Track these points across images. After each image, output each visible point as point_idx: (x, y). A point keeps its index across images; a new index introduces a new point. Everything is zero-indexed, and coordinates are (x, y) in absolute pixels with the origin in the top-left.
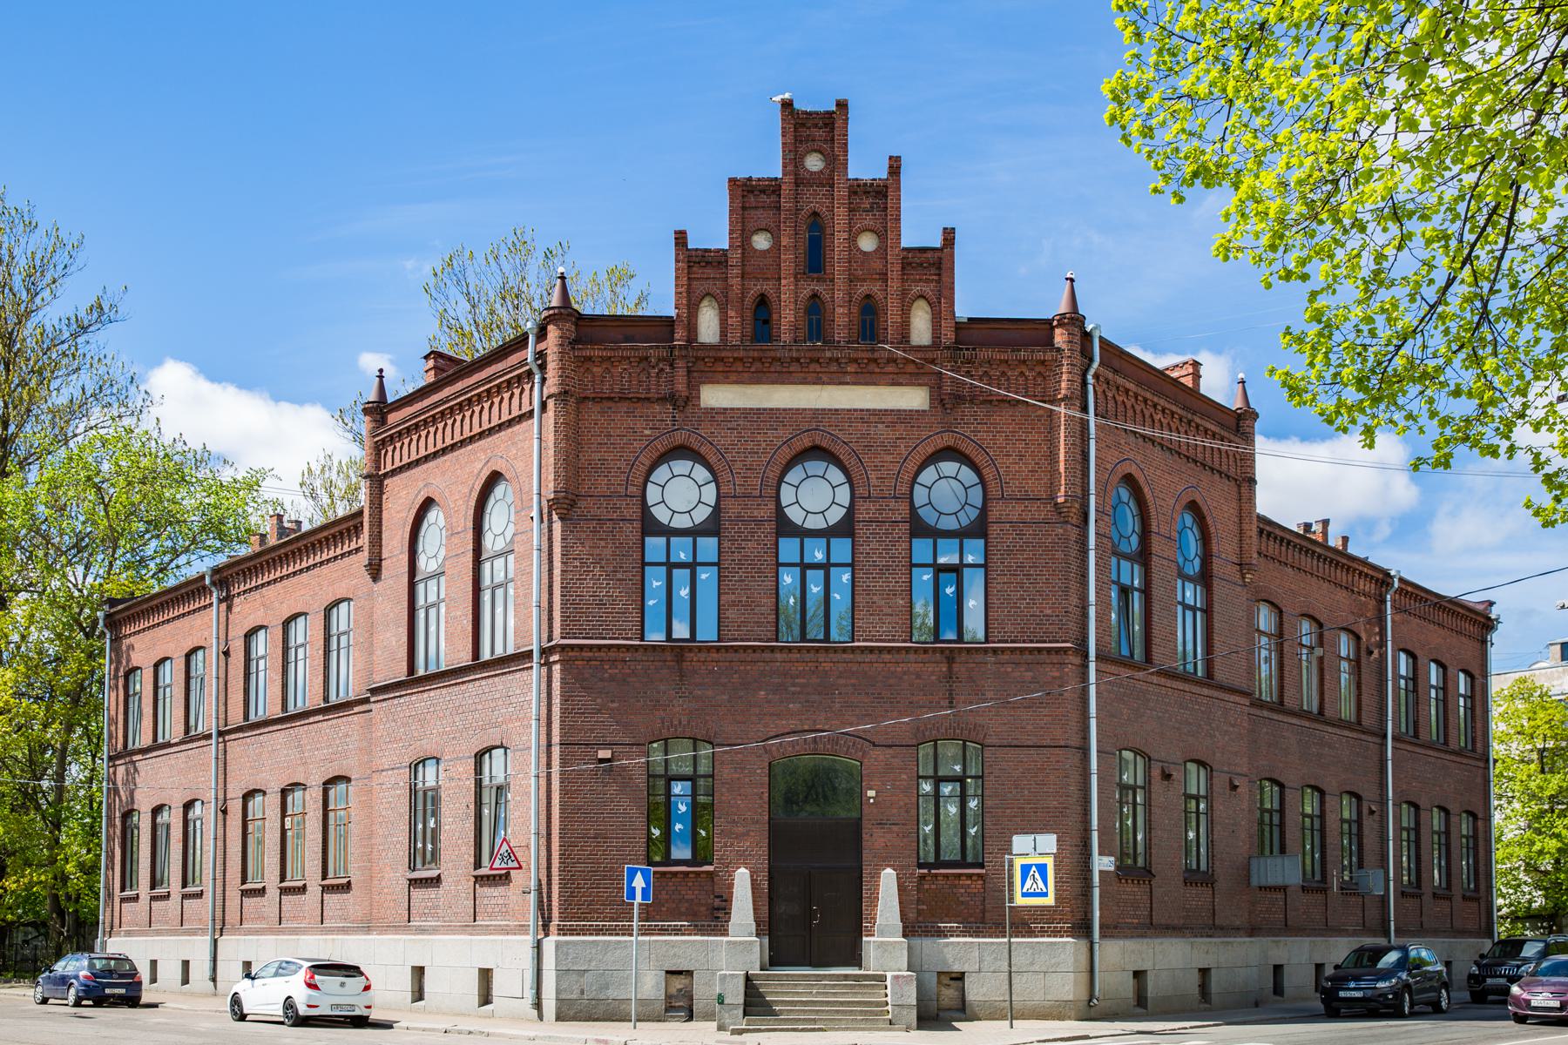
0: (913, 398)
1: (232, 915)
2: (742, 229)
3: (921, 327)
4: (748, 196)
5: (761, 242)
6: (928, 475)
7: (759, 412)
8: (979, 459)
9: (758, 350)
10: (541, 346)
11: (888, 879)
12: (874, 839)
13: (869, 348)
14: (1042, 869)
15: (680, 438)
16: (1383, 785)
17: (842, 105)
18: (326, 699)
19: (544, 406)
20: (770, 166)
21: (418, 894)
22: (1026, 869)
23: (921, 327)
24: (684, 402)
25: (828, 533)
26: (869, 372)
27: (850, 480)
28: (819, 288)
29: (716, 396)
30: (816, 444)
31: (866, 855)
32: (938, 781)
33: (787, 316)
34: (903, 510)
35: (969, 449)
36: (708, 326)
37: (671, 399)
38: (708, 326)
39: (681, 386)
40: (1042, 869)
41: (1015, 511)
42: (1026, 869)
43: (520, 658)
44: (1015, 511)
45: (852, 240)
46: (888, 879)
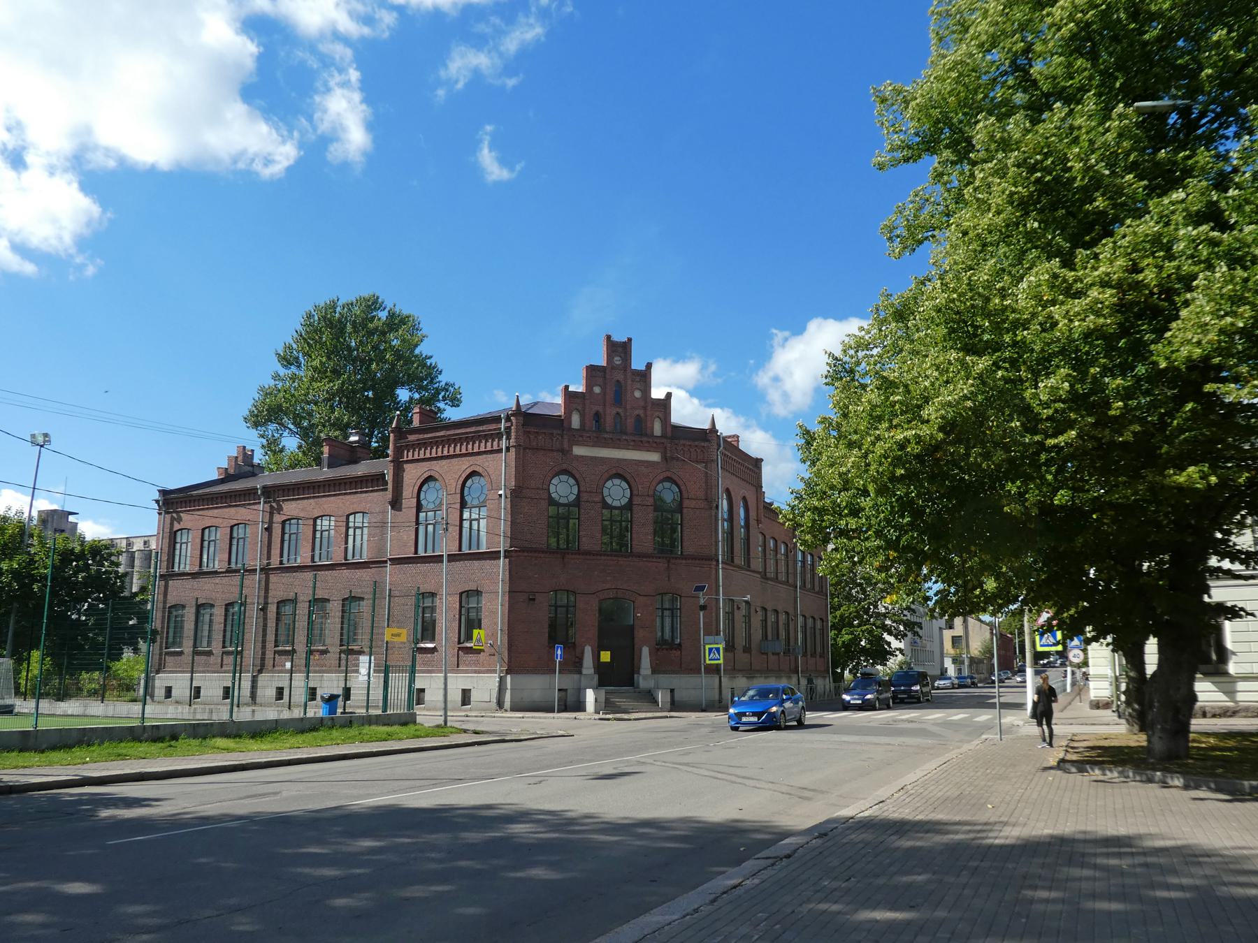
0: (654, 457)
1: (269, 662)
2: (589, 386)
3: (657, 429)
4: (593, 372)
5: (597, 390)
6: (609, 484)
7: (596, 458)
8: (680, 483)
9: (597, 432)
10: (508, 424)
11: (645, 651)
12: (640, 634)
13: (641, 437)
14: (718, 650)
15: (564, 466)
16: (796, 608)
17: (630, 340)
18: (313, 560)
19: (508, 449)
20: (602, 362)
21: (419, 656)
22: (710, 650)
23: (657, 429)
24: (566, 452)
25: (620, 508)
26: (638, 446)
27: (578, 484)
28: (620, 411)
29: (578, 451)
30: (619, 471)
31: (636, 640)
32: (663, 610)
33: (609, 421)
34: (545, 496)
35: (574, 472)
36: (576, 421)
37: (562, 451)
38: (576, 421)
39: (566, 446)
40: (718, 650)
41: (693, 504)
42: (710, 650)
43: (494, 555)
44: (693, 504)
45: (604, 393)
46: (645, 651)
